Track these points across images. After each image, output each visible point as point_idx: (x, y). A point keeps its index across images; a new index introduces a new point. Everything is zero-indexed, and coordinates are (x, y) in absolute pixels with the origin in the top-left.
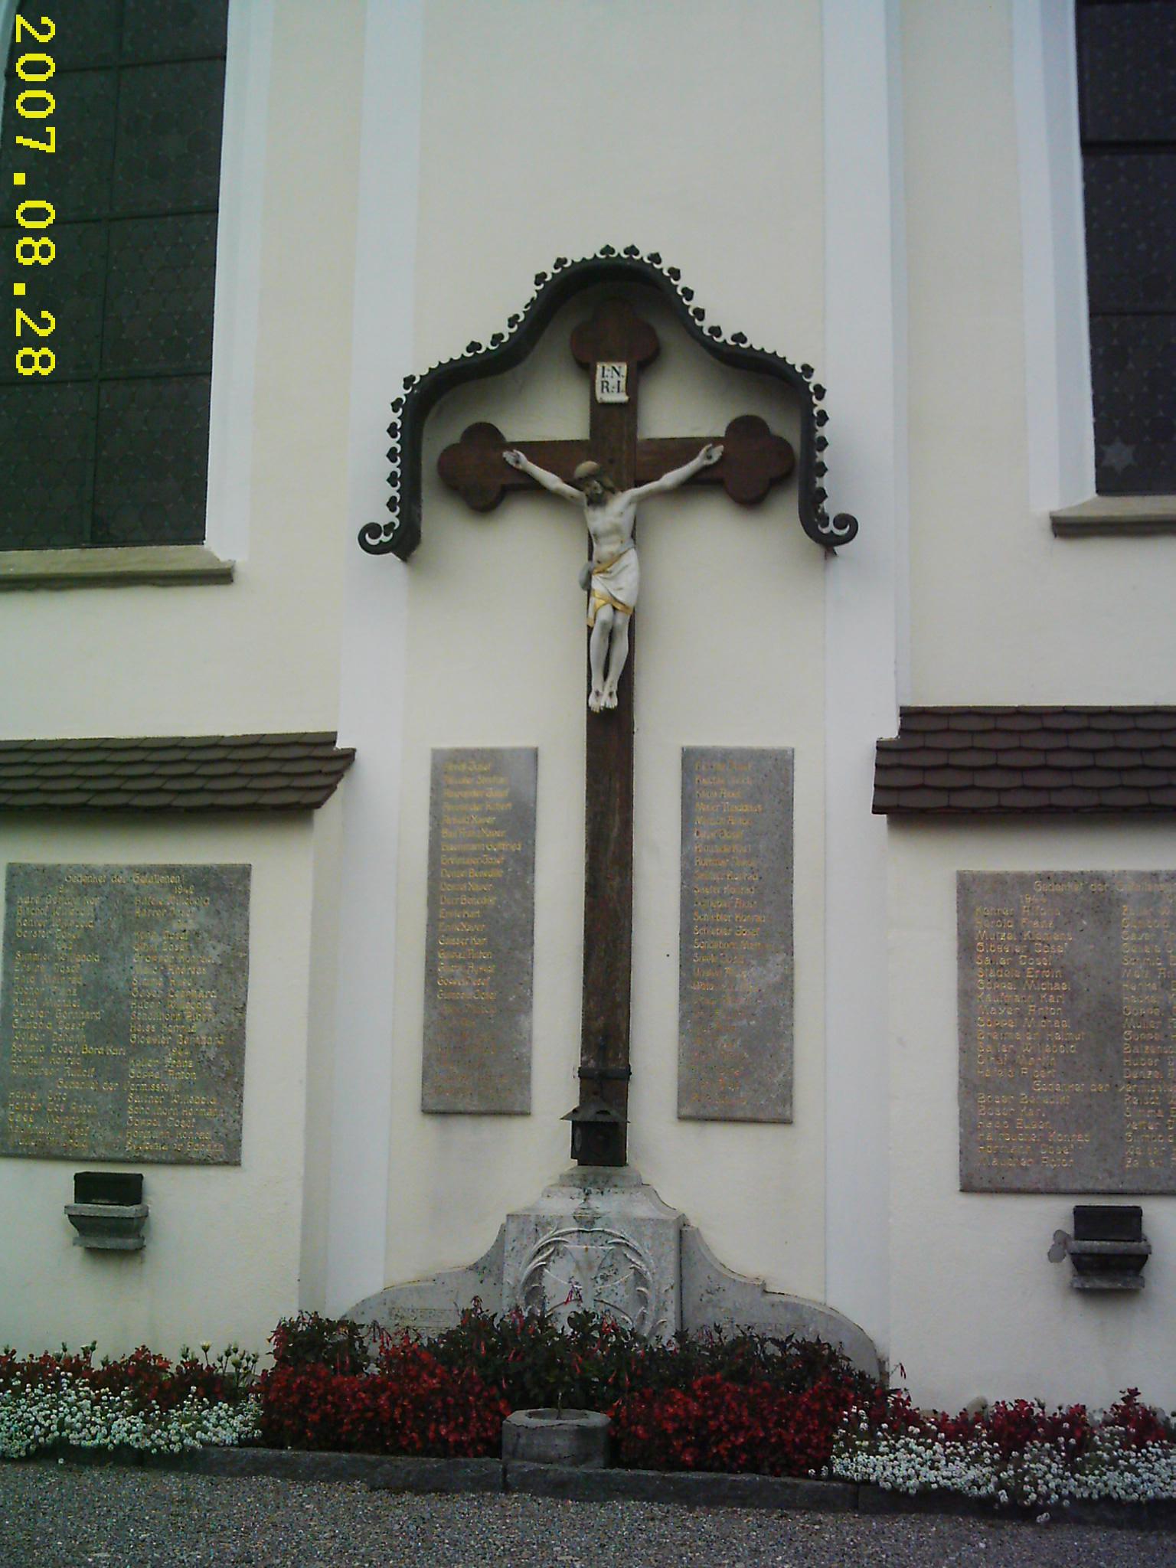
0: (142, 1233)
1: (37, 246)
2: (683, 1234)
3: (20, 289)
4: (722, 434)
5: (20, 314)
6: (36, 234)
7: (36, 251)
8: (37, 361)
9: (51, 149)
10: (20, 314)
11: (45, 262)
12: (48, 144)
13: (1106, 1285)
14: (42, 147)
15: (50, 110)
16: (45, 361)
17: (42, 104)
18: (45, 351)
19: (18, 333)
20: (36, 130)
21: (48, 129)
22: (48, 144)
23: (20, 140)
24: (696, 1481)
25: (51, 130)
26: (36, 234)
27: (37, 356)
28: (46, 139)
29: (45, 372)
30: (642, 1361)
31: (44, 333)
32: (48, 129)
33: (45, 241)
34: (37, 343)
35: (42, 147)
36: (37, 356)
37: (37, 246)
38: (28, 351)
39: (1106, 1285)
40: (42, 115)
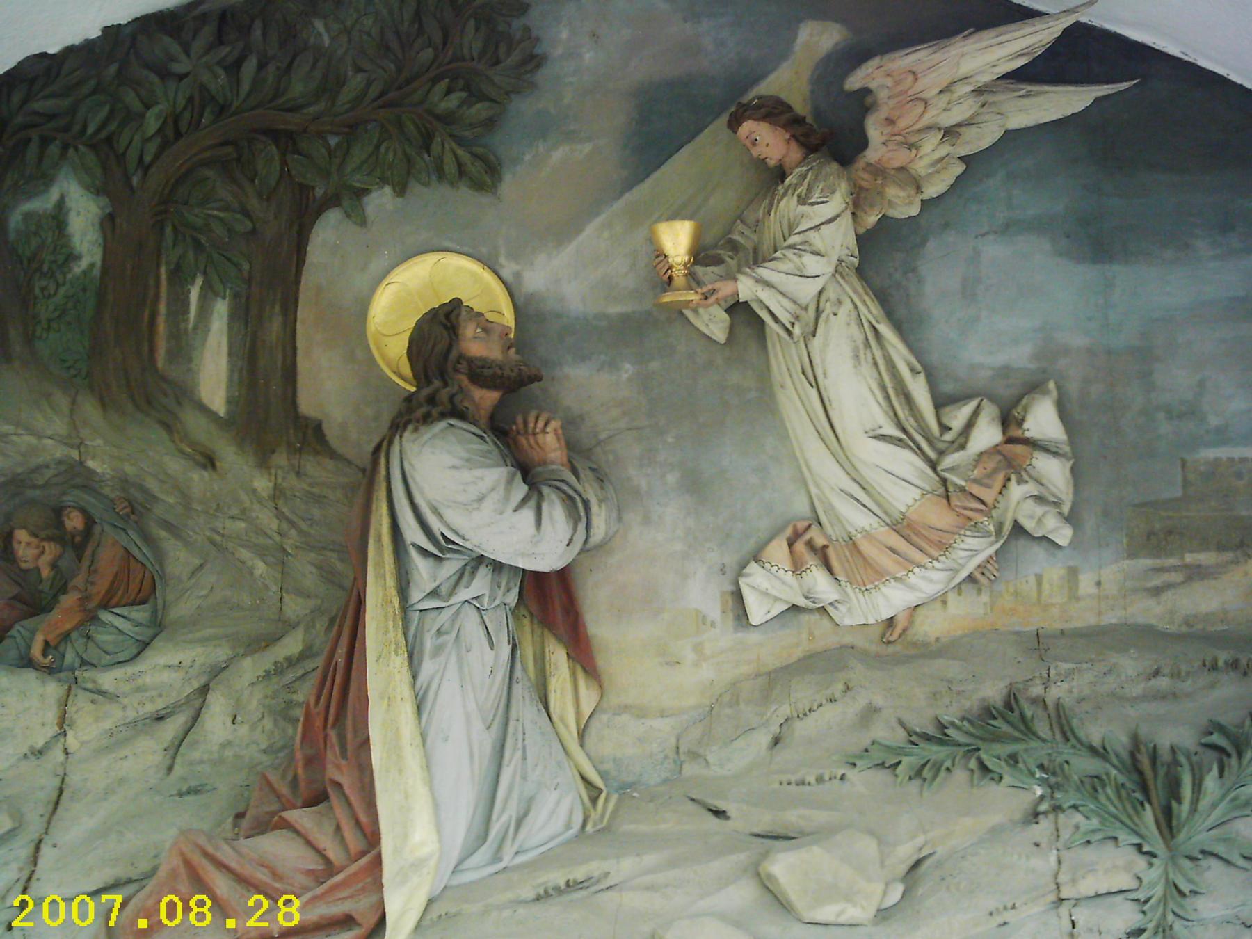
0: (75, 253)
1: (196, 910)
2: (1155, 747)
5: (251, 923)
6: (187, 910)
8: (201, 910)
10: (251, 923)
11: (209, 903)
12: (115, 900)
13: (1033, 29)
18: (192, 903)
19: (31, 924)
21: (103, 901)
22: (115, 900)
26: (187, 910)
32: (103, 901)
33: (280, 903)
35: (117, 905)
38: (280, 917)
39: (1033, 29)
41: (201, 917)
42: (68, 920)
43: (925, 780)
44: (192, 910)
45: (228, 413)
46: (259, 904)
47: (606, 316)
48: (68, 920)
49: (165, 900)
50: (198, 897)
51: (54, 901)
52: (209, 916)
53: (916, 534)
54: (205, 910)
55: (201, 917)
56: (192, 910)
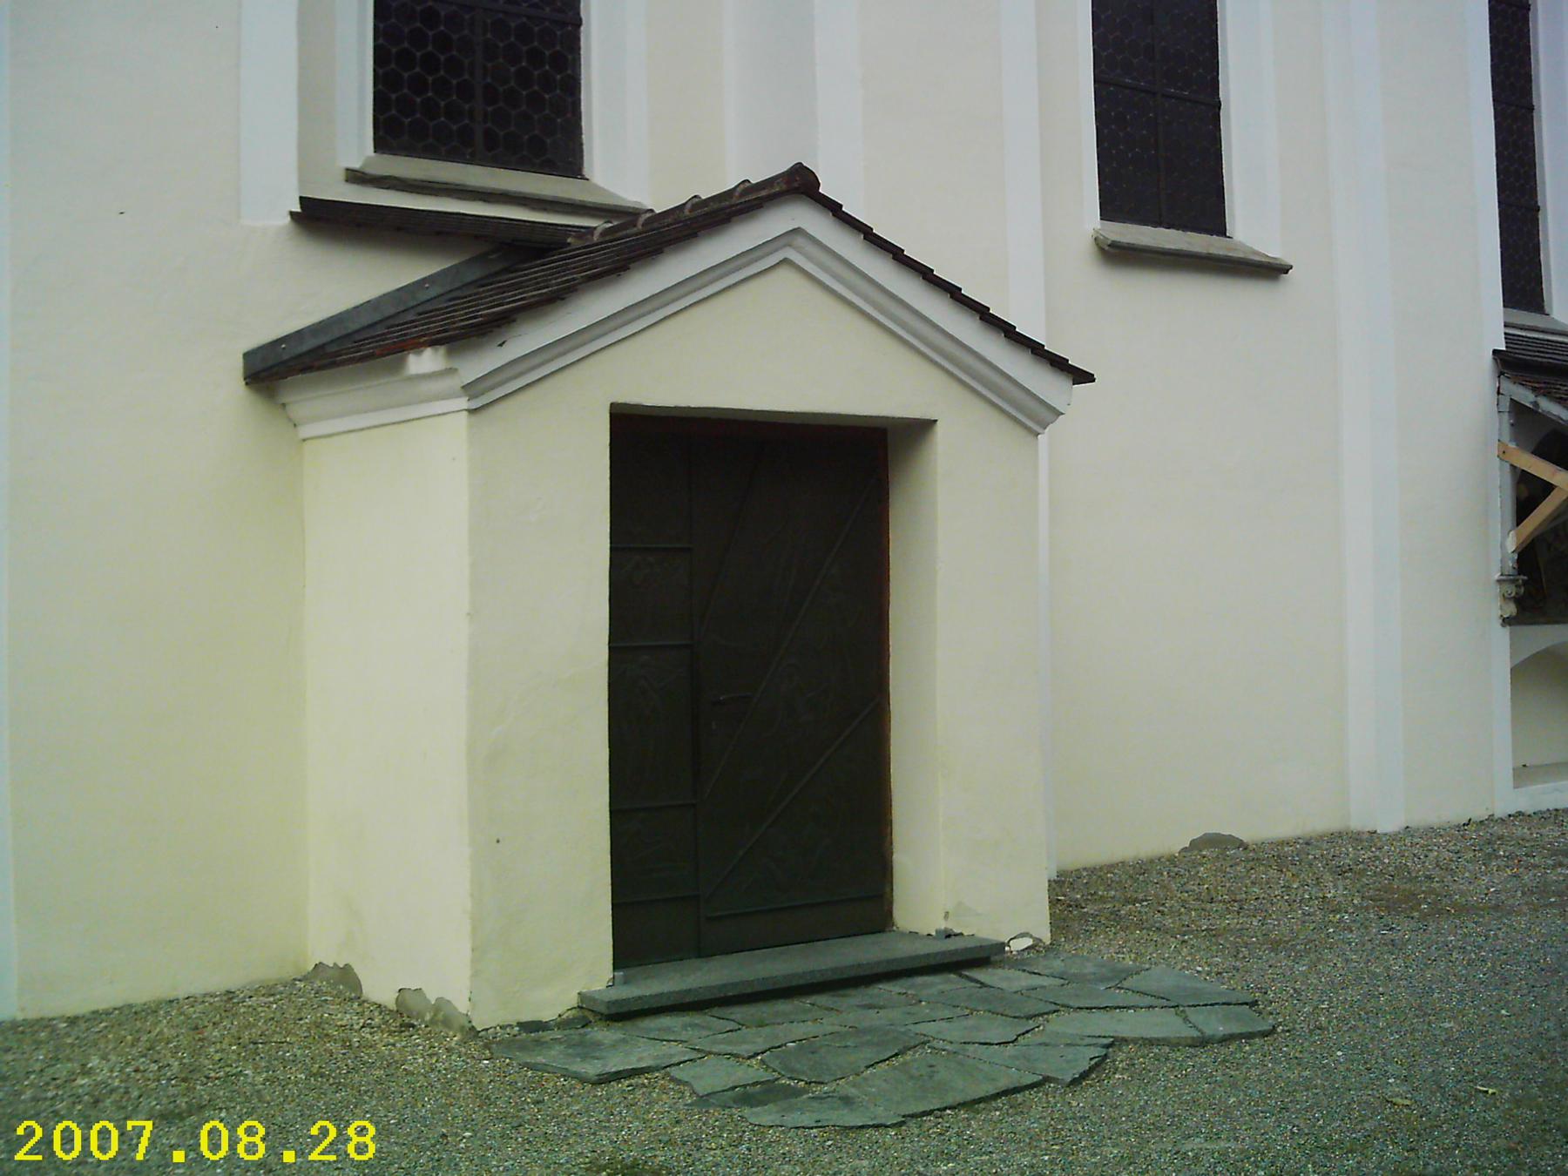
11: (372, 1130)
15: (110, 1126)
16: (362, 1131)
17: (215, 1147)
23: (140, 1157)
27: (356, 1139)
31: (333, 1133)
34: (342, 1138)
36: (356, 1139)
40: (115, 1134)
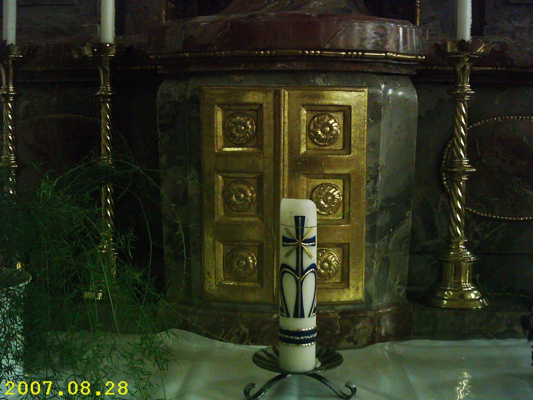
1: (84, 387)
3: (98, 393)
4: (342, 180)
6: (80, 388)
7: (85, 387)
9: (51, 383)
14: (50, 386)
20: (44, 388)
24: (454, 125)
25: (44, 383)
26: (80, 388)
28: (47, 385)
29: (89, 385)
30: (370, 309)
33: (119, 385)
34: (117, 387)
35: (50, 386)
37: (84, 387)
40: (39, 386)
41: (85, 391)
42: (29, 392)
43: (373, 247)
44: (89, 388)
45: (365, 300)
46: (110, 385)
47: (390, 215)
48: (29, 392)
49: (70, 383)
50: (84, 382)
51: (23, 384)
52: (89, 390)
53: (410, 33)
54: (87, 387)
55: (123, 390)
56: (89, 388)
